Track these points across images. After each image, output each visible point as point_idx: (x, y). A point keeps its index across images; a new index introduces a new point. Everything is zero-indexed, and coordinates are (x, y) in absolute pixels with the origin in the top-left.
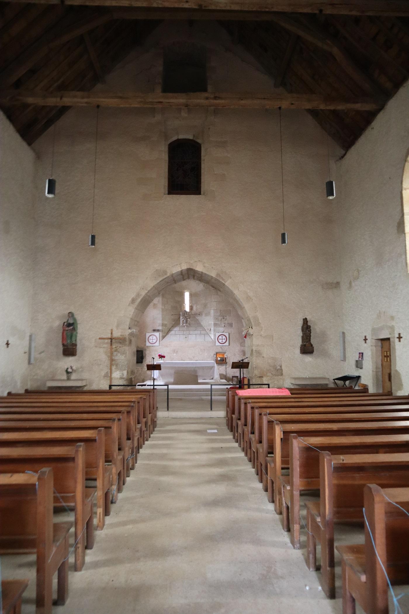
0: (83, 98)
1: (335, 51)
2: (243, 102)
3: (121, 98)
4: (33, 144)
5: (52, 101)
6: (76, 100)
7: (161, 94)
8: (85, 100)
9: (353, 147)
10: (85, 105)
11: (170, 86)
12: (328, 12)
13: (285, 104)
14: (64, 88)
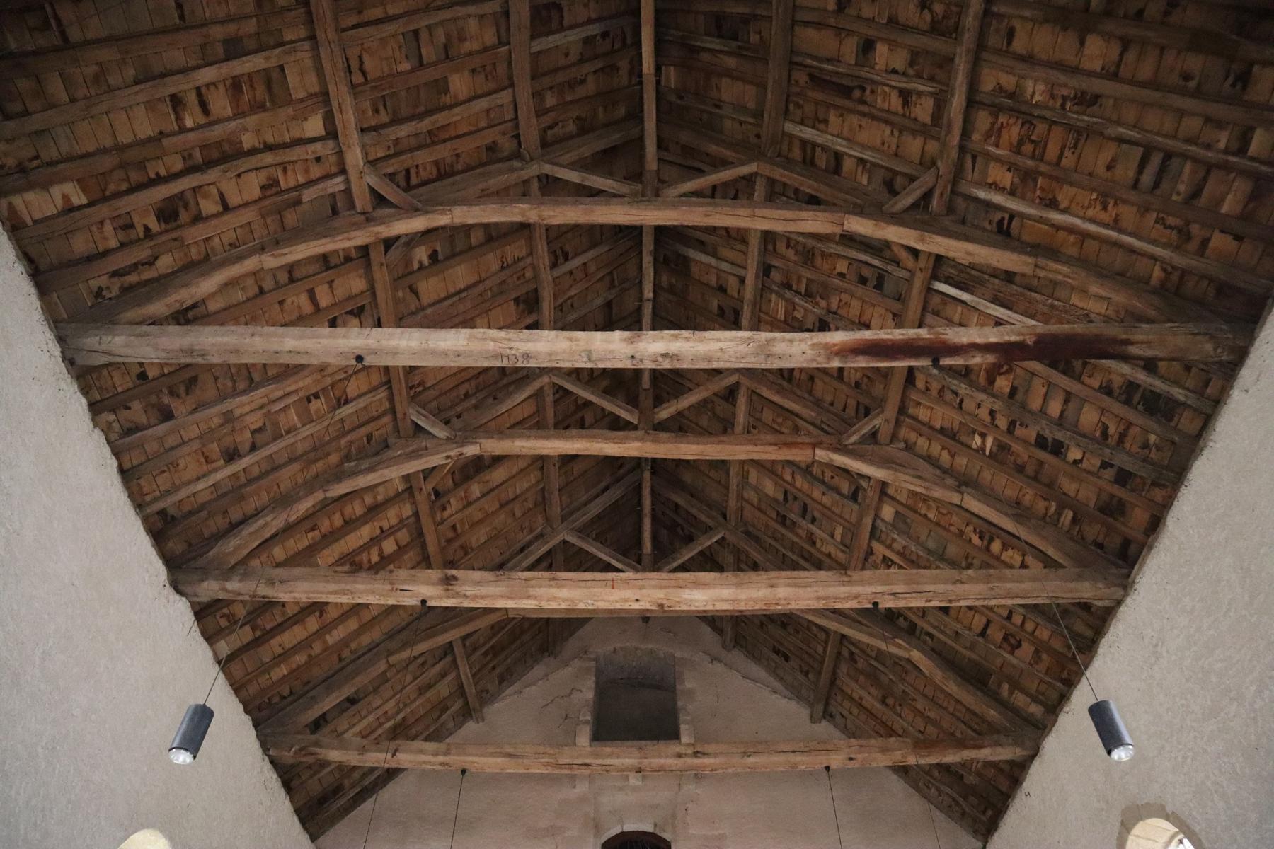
0: (436, 754)
1: (916, 655)
2: (752, 760)
3: (509, 755)
4: (321, 839)
5: (376, 759)
6: (422, 758)
7: (589, 749)
8: (441, 758)
9: (996, 835)
10: (440, 768)
11: (608, 729)
12: (890, 604)
13: (836, 760)
14: (401, 732)
